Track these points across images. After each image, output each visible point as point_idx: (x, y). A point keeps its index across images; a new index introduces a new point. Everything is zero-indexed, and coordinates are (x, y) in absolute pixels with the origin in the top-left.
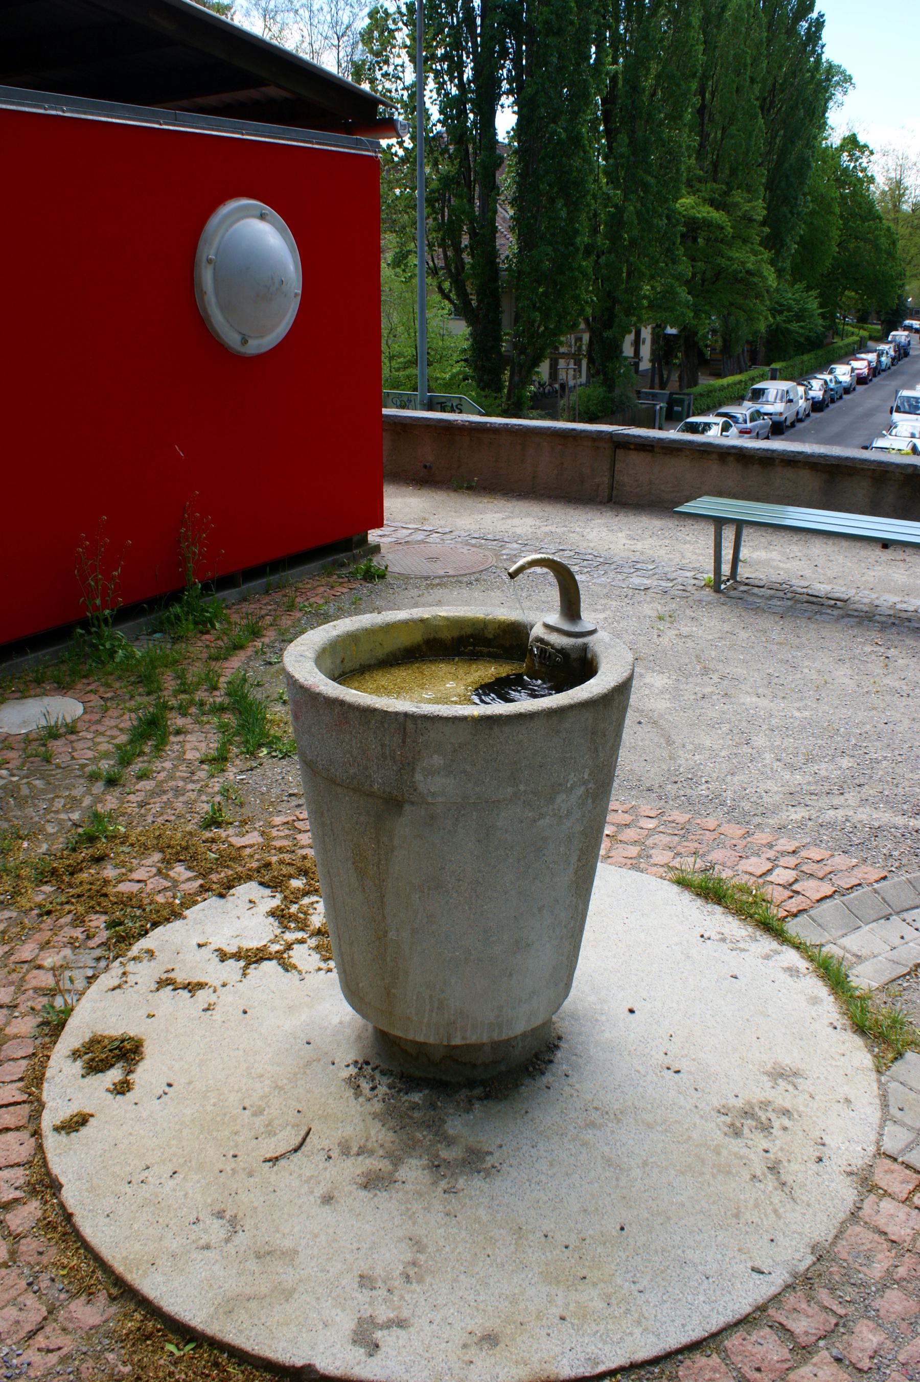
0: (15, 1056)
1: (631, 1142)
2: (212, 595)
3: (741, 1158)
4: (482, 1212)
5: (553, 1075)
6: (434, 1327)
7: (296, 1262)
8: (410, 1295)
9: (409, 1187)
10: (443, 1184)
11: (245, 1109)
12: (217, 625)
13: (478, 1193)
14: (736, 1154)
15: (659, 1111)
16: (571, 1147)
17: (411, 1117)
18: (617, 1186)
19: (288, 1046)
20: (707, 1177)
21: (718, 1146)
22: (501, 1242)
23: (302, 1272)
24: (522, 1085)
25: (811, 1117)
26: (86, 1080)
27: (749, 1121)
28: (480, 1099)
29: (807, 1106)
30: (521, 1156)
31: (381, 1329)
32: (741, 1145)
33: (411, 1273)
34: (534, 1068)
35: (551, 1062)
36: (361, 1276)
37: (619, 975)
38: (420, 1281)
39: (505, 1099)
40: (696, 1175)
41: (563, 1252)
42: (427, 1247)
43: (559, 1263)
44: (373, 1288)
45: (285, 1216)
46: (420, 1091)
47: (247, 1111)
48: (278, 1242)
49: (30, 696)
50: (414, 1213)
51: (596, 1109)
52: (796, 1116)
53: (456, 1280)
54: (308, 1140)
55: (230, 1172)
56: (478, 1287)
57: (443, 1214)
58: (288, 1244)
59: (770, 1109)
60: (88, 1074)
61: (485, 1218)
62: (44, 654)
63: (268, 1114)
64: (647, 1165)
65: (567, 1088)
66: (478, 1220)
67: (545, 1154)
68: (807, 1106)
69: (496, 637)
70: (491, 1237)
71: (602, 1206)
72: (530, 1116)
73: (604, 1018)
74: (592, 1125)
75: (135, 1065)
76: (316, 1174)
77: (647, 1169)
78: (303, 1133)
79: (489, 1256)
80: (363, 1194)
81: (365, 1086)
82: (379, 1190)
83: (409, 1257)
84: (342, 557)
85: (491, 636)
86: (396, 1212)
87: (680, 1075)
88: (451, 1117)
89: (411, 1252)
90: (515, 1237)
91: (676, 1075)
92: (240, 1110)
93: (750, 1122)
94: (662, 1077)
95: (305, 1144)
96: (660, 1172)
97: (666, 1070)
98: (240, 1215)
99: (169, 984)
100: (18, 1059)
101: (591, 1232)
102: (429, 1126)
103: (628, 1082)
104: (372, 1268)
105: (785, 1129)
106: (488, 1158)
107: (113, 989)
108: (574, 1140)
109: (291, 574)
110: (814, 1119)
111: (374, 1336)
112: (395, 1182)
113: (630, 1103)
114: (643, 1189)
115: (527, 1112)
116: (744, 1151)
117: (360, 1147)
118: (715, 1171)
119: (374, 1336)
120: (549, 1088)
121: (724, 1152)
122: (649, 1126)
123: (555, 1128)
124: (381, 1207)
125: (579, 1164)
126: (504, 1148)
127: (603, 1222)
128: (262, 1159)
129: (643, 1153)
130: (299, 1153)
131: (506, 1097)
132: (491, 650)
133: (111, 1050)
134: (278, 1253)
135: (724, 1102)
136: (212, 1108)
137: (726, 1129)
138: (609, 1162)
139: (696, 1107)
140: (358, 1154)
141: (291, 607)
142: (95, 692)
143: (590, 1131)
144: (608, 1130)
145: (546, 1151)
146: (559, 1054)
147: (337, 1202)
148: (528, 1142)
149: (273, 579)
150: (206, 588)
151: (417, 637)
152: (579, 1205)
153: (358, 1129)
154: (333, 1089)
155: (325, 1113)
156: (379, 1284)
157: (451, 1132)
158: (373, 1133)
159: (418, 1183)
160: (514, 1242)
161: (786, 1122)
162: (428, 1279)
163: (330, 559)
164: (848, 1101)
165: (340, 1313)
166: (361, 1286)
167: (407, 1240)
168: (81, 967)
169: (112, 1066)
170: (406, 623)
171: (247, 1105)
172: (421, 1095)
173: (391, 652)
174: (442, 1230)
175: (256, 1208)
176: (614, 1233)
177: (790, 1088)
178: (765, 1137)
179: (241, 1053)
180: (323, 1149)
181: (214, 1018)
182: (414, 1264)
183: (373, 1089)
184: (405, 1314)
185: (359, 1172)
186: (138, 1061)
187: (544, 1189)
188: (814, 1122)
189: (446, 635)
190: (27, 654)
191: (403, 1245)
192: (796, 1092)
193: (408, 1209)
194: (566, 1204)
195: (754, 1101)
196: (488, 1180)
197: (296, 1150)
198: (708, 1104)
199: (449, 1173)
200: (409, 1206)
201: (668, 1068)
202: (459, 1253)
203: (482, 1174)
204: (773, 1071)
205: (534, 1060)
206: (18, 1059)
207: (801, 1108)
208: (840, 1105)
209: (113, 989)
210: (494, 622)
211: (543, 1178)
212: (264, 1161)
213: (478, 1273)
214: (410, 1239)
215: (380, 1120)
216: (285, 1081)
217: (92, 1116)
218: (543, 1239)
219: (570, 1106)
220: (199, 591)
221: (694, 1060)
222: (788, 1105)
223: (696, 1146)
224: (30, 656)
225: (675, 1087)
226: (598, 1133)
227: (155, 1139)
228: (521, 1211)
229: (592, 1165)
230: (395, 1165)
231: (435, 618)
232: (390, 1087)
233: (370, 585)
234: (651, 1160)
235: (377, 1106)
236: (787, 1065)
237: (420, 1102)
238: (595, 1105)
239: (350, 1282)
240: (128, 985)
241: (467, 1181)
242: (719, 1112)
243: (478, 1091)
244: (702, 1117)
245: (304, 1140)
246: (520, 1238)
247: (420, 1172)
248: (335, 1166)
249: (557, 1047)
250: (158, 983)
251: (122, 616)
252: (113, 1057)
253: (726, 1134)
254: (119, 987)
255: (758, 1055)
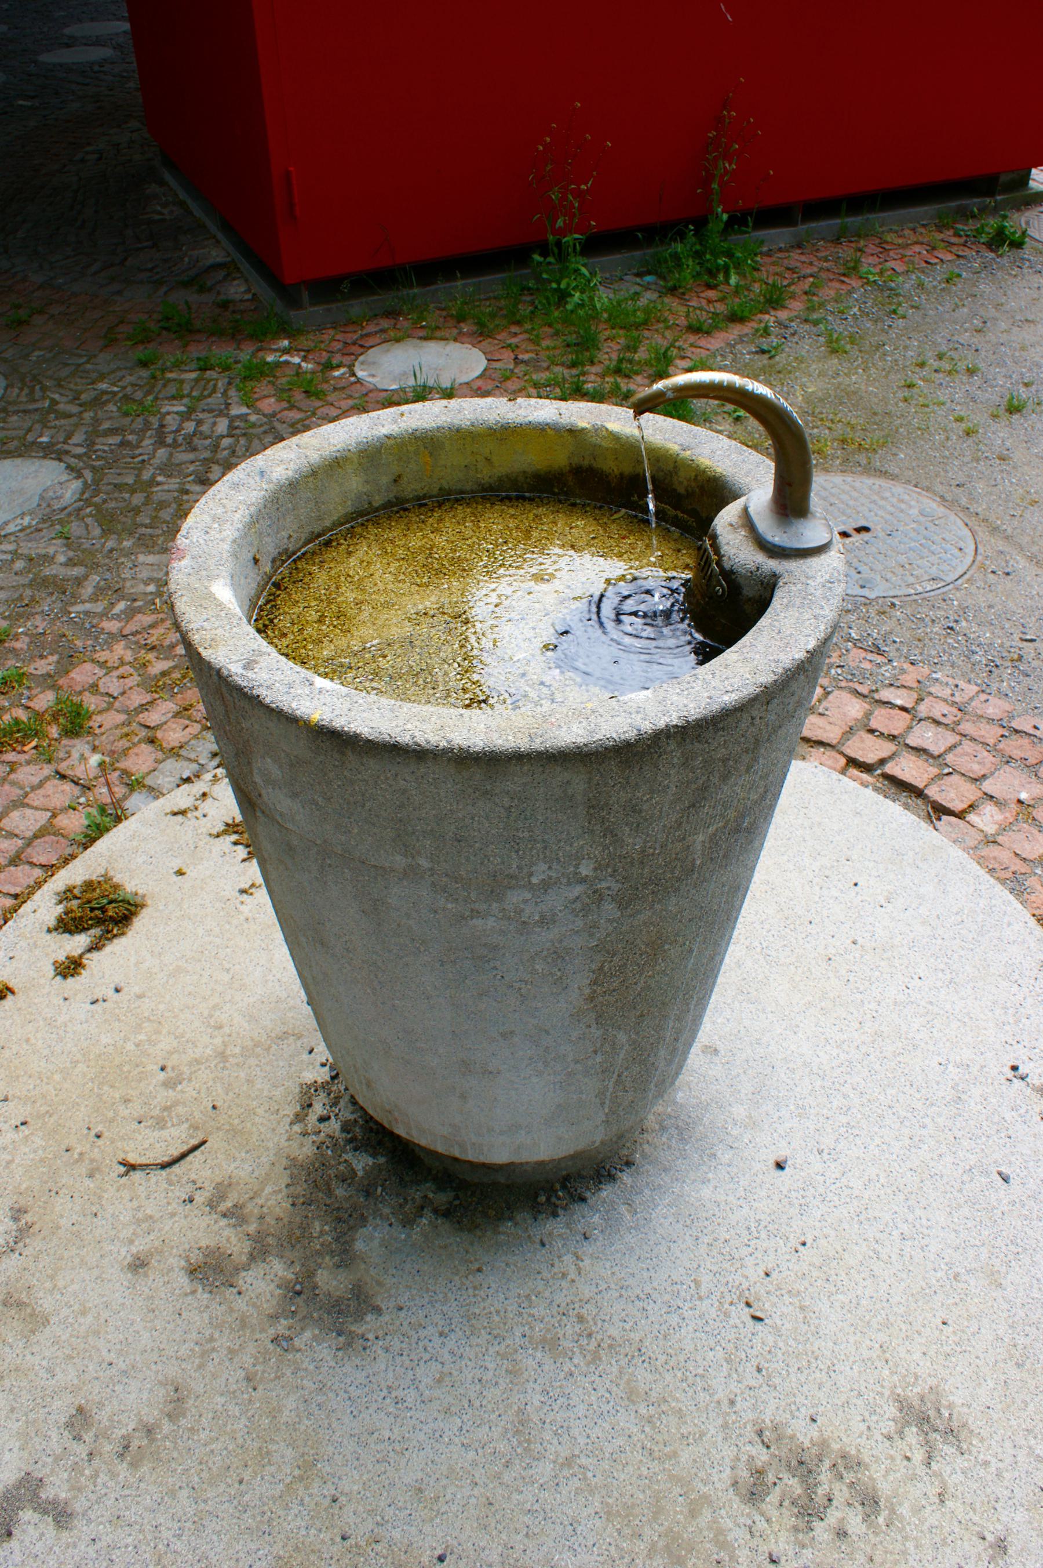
0: (35, 860)
1: (581, 1409)
2: (746, 233)
3: (723, 1545)
4: (291, 1402)
5: (568, 1226)
6: (91, 1550)
7: (34, 1339)
8: (107, 1478)
9: (241, 1304)
10: (282, 1326)
11: (163, 1069)
12: (733, 280)
13: (311, 1367)
14: (720, 1532)
15: (668, 1377)
16: (491, 1366)
17: (329, 1192)
18: (498, 1476)
19: (284, 995)
20: (642, 1546)
21: (706, 1499)
22: (273, 1469)
23: (29, 1357)
24: (511, 1219)
25: (906, 1538)
26: (48, 937)
27: (793, 1482)
28: (436, 1211)
29: (917, 1510)
30: (414, 1340)
31: (35, 1509)
32: (741, 1520)
33: (135, 1444)
34: (548, 1199)
35: (583, 1200)
36: (80, 1410)
37: (819, 1083)
38: (134, 1465)
39: (470, 1231)
40: (627, 1531)
41: (333, 1543)
42: (184, 1416)
43: (312, 1558)
44: (77, 1438)
45: (77, 1260)
46: (374, 1155)
47: (163, 1074)
48: (41, 1294)
49: (436, 339)
50: (213, 1349)
51: (581, 1319)
52: (881, 1520)
53: (172, 1493)
54: (190, 1158)
55: (76, 1156)
56: (188, 1524)
57: (243, 1374)
58: (47, 1303)
59: (849, 1477)
60: (56, 929)
61: (286, 1416)
62: (493, 281)
63: (182, 1092)
64: (570, 1466)
65: (568, 1259)
66: (274, 1414)
67: (447, 1356)
68: (917, 1510)
69: (690, 494)
70: (268, 1453)
71: (449, 1497)
72: (480, 1277)
73: (726, 1156)
74: (551, 1344)
75: (109, 939)
76: (157, 1216)
77: (566, 1472)
78: (194, 1142)
79: (241, 1482)
80: (183, 1280)
81: (319, 1108)
82: (204, 1286)
83: (151, 1415)
84: (974, 203)
85: (681, 490)
86: (194, 1335)
87: (759, 1326)
88: (378, 1221)
89: (161, 1411)
90: (297, 1472)
91: (750, 1322)
92: (157, 1068)
93: (794, 1485)
94: (727, 1315)
95: (182, 1162)
96: (578, 1491)
97: (743, 1305)
98: (36, 1227)
99: (236, 832)
100: (36, 865)
101: (396, 1534)
102: (339, 1220)
103: (667, 1297)
104: (101, 1405)
105: (842, 1534)
106: (369, 1318)
107: (175, 814)
108: (504, 1356)
109: (876, 218)
110: (910, 1545)
111: (21, 1513)
112: (231, 1286)
113: (635, 1336)
114: (528, 1506)
115: (479, 1270)
116: (738, 1535)
117: (235, 1206)
118: (661, 1544)
119: (21, 1513)
120: (543, 1245)
121: (706, 1516)
122: (631, 1396)
123: (496, 1319)
124: (185, 1314)
125: (477, 1403)
126: (402, 1314)
127: (427, 1529)
128: (121, 1156)
129: (582, 1440)
130: (164, 1173)
131: (473, 1228)
132: (680, 515)
133: (92, 909)
134: (29, 1311)
135: (783, 1417)
136: (133, 1047)
137: (745, 1474)
138: (522, 1420)
139: (732, 1403)
140: (224, 1215)
141: (852, 269)
142: (514, 348)
143: (539, 1355)
144: (568, 1366)
145: (452, 1353)
146: (607, 1192)
147: (146, 1275)
148: (441, 1323)
149: (853, 221)
150: (737, 222)
151: (560, 459)
152: (420, 1475)
153: (256, 1174)
154: (278, 1093)
155: (240, 1127)
156: (88, 1437)
157: (359, 1246)
158: (268, 1189)
159: (254, 1305)
160: (289, 1480)
161: (855, 1523)
162: (145, 1469)
163: (953, 204)
164: (1001, 1546)
165: (15, 1450)
166: (69, 1425)
167: (171, 1388)
168: (190, 760)
169: (85, 930)
170: (541, 430)
171: (169, 1065)
172: (370, 1161)
173: (507, 476)
174: (221, 1400)
175: (58, 1228)
176: (425, 1559)
177: (918, 1456)
178: (796, 1529)
179: (226, 977)
180: (194, 1182)
181: (242, 908)
182: (150, 1431)
183: (323, 1119)
184: (78, 1506)
185: (203, 1243)
186: (115, 936)
187: (396, 1417)
188: (904, 1553)
189: (610, 466)
190: (455, 279)
191: (163, 1392)
192: (921, 1471)
193: (211, 1339)
194: (404, 1461)
195: (835, 1446)
196: (340, 1354)
197: (164, 1166)
198: (754, 1407)
199: (303, 1311)
200: (217, 1335)
201: (748, 1305)
202: (212, 1451)
203: (341, 1339)
204: (916, 1403)
205: (558, 1186)
206: (36, 865)
207: (904, 1510)
208: (981, 1546)
209: (175, 814)
210: (689, 466)
211: (411, 1396)
212: (121, 1163)
213: (205, 1501)
214: (176, 1390)
215: (291, 1176)
216: (237, 1050)
217: (13, 992)
218: (327, 1502)
219: (547, 1294)
220: (722, 226)
221: (802, 1308)
222: (885, 1488)
223: (672, 1478)
224: (459, 283)
225: (730, 1347)
226: (548, 1365)
227: (43, 1063)
228: (338, 1434)
229: (493, 1417)
230: (252, 1257)
231: (597, 430)
232: (346, 1128)
233: (992, 255)
234: (583, 1461)
235: (306, 1150)
236: (950, 1406)
237: (360, 1174)
238: (584, 1311)
239: (62, 1407)
240: (196, 814)
241: (315, 1338)
242: (760, 1433)
243: (442, 1199)
244: (725, 1426)
245: (183, 1156)
246: (301, 1478)
247: (273, 1286)
248: (186, 1217)
249: (612, 1178)
250: (227, 825)
251: (594, 246)
252: (91, 919)
253: (735, 1484)
254: (183, 813)
255: (917, 1356)
